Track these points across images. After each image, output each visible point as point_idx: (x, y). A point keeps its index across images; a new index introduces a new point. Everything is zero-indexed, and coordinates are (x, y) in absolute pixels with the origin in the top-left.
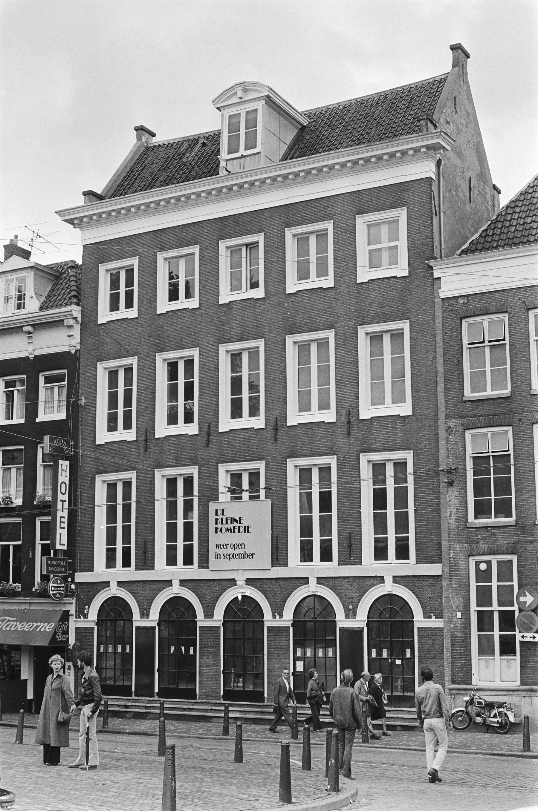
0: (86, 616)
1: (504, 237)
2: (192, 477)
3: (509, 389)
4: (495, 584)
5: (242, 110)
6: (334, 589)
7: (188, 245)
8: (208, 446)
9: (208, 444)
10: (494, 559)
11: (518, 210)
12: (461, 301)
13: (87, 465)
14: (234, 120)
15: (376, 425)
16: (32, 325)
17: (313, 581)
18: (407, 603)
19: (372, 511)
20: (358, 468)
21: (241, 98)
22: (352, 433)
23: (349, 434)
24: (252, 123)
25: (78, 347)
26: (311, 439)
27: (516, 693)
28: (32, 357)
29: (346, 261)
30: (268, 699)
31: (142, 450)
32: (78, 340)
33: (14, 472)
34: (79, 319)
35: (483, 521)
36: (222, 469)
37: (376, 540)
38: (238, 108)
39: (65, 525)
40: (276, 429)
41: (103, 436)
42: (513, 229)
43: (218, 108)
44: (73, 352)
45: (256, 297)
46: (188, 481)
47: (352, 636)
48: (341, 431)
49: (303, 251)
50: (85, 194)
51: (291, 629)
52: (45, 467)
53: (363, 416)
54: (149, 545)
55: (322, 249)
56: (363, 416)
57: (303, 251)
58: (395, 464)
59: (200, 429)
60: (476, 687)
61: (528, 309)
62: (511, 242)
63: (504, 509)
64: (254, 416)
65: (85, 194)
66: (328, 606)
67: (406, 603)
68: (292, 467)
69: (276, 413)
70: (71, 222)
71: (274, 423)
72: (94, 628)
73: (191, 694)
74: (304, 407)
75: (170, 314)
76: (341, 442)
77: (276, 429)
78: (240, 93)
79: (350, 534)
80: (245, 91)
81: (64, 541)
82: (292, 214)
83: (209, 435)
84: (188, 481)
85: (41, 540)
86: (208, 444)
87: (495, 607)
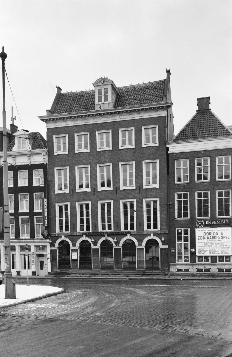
0: (54, 246)
1: (187, 135)
2: (68, 206)
3: (188, 181)
4: (183, 236)
5: (103, 88)
6: (70, 239)
7: (85, 131)
8: (94, 195)
9: (94, 195)
10: (183, 229)
11: (190, 127)
12: (175, 155)
13: (53, 199)
14: (106, 90)
15: (148, 190)
16: (14, 155)
17: (152, 235)
18: (158, 242)
19: (123, 216)
20: (142, 203)
21: (102, 84)
22: (140, 192)
23: (140, 193)
24: (106, 92)
25: (47, 162)
26: (128, 193)
27: (227, 265)
28: (30, 165)
29: (138, 140)
30: (146, 269)
31: (72, 196)
32: (47, 160)
33: (24, 201)
34: (47, 153)
35: (222, 217)
36: (99, 202)
37: (147, 223)
38: (101, 87)
39: (47, 219)
40: (116, 191)
41: (57, 192)
42: (189, 133)
43: (94, 86)
44: (45, 164)
45: (132, 148)
46: (66, 207)
47: (118, 250)
48: (137, 192)
49: (124, 136)
50: (47, 111)
51: (122, 249)
52: (36, 200)
53: (77, 191)
54: (96, 226)
55: (130, 136)
56: (77, 191)
57: (124, 136)
58: (153, 202)
59: (91, 190)
60: (218, 264)
61: (195, 158)
62: (194, 137)
63: (186, 215)
64: (109, 186)
65: (47, 111)
66: (133, 243)
67: (82, 242)
68: (99, 203)
69: (139, 184)
70: (43, 120)
71: (116, 189)
72: (56, 250)
73: (90, 268)
74: (125, 183)
75: (80, 154)
76: (137, 195)
77: (116, 191)
78: (102, 82)
79: (140, 222)
80: (104, 81)
81: (47, 224)
82: (121, 124)
83: (94, 192)
84: (66, 207)
85: (36, 223)
86: (94, 195)
87: (183, 242)
